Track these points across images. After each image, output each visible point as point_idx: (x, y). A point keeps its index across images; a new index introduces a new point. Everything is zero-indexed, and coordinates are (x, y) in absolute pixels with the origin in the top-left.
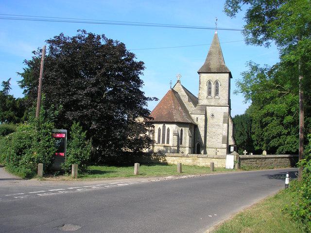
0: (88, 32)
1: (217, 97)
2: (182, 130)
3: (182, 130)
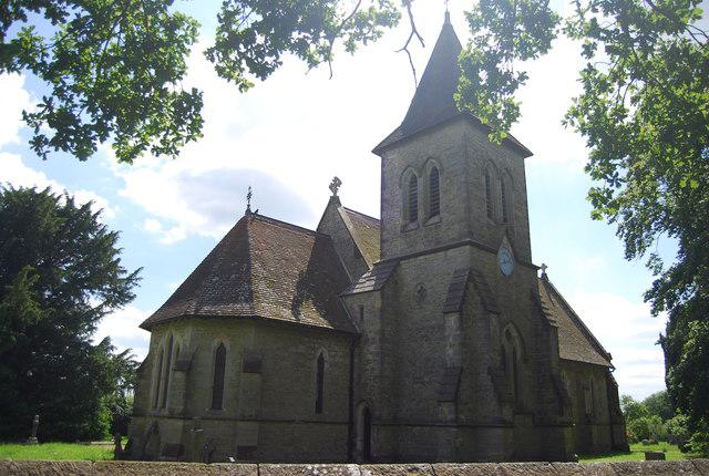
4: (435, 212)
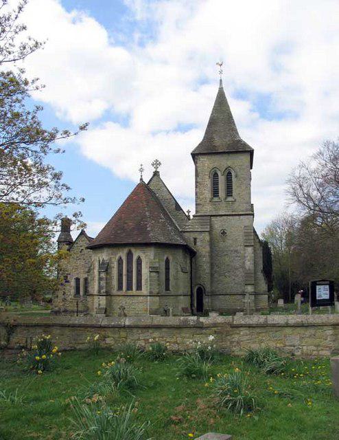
1: (230, 199)
2: (167, 262)
3: (167, 262)
4: (229, 192)
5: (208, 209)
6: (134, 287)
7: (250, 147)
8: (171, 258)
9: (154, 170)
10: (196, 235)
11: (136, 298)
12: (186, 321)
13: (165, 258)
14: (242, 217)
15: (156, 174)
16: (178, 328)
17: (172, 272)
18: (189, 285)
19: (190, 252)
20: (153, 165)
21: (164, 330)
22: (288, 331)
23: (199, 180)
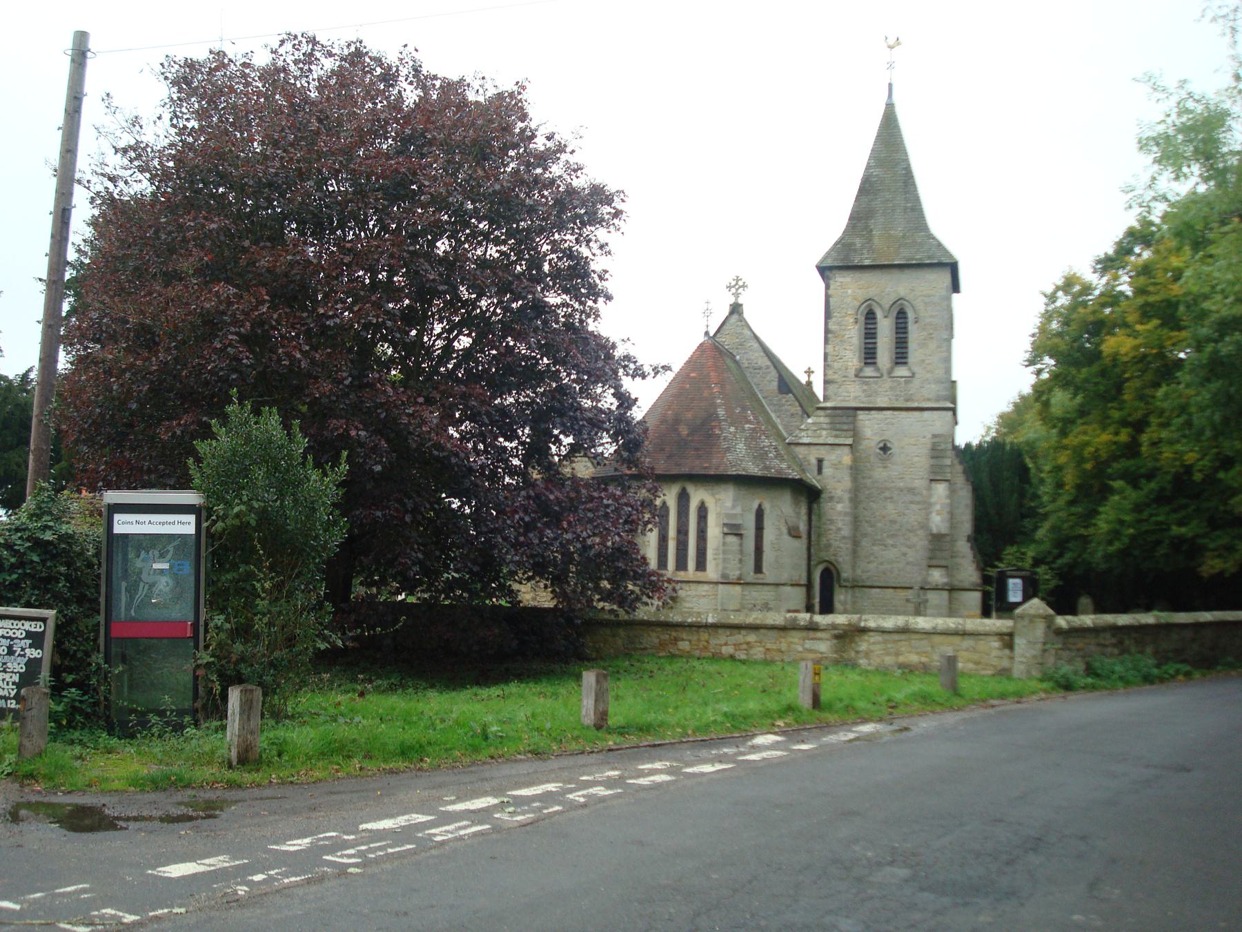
0: (160, 111)
1: (902, 371)
2: (760, 514)
3: (760, 514)
4: (901, 356)
5: (852, 394)
6: (691, 564)
7: (951, 256)
8: (767, 506)
9: (732, 300)
10: (822, 452)
11: (693, 586)
12: (795, 619)
13: (755, 506)
14: (926, 414)
15: (736, 309)
16: (783, 629)
17: (769, 535)
18: (804, 563)
19: (809, 494)
20: (729, 287)
21: (762, 631)
22: (937, 639)
23: (832, 327)
